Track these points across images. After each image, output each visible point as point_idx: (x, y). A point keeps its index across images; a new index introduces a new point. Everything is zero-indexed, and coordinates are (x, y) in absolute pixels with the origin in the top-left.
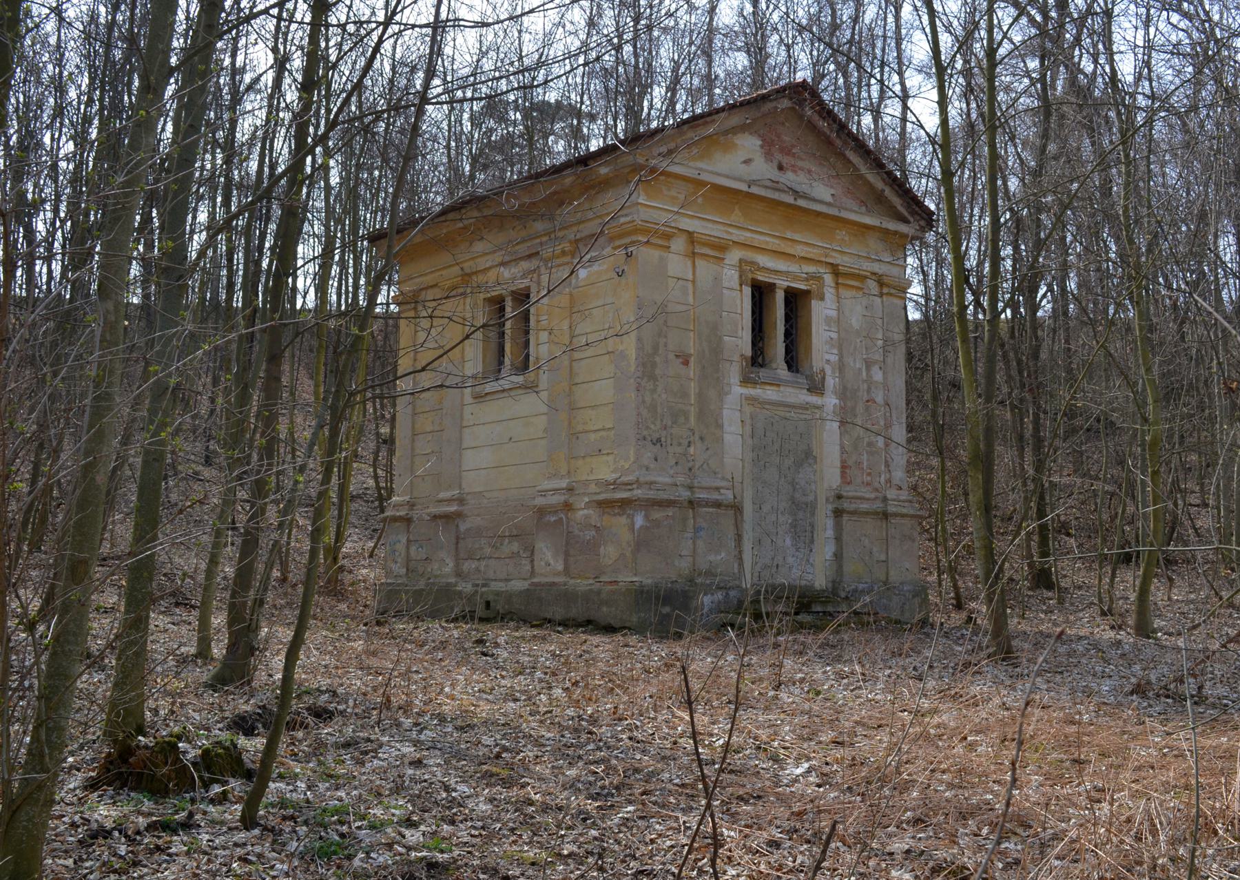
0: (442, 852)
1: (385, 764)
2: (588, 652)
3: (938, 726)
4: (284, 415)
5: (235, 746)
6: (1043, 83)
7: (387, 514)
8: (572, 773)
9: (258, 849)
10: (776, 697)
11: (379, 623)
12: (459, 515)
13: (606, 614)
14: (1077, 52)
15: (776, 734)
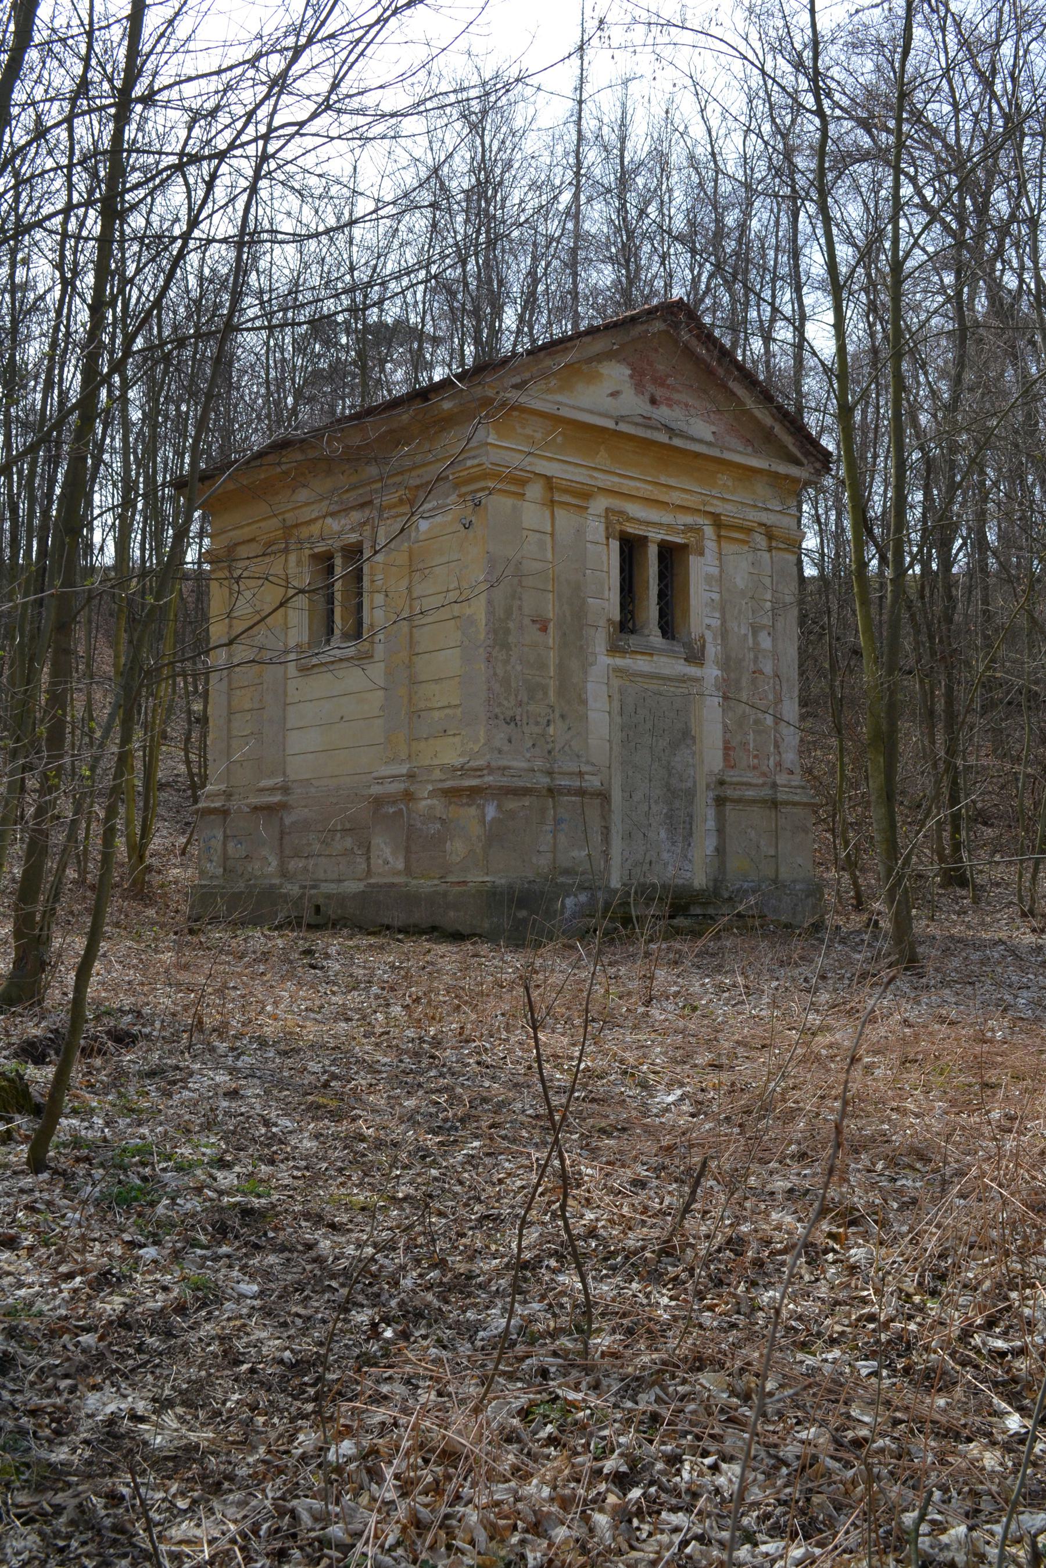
0: (259, 1196)
1: (196, 1095)
2: (432, 964)
3: (830, 1046)
4: (80, 690)
5: (21, 1077)
6: (959, 304)
7: (200, 805)
8: (410, 1103)
9: (46, 1196)
10: (646, 1014)
11: (191, 932)
12: (283, 806)
13: (452, 919)
14: (999, 266)
15: (645, 1056)
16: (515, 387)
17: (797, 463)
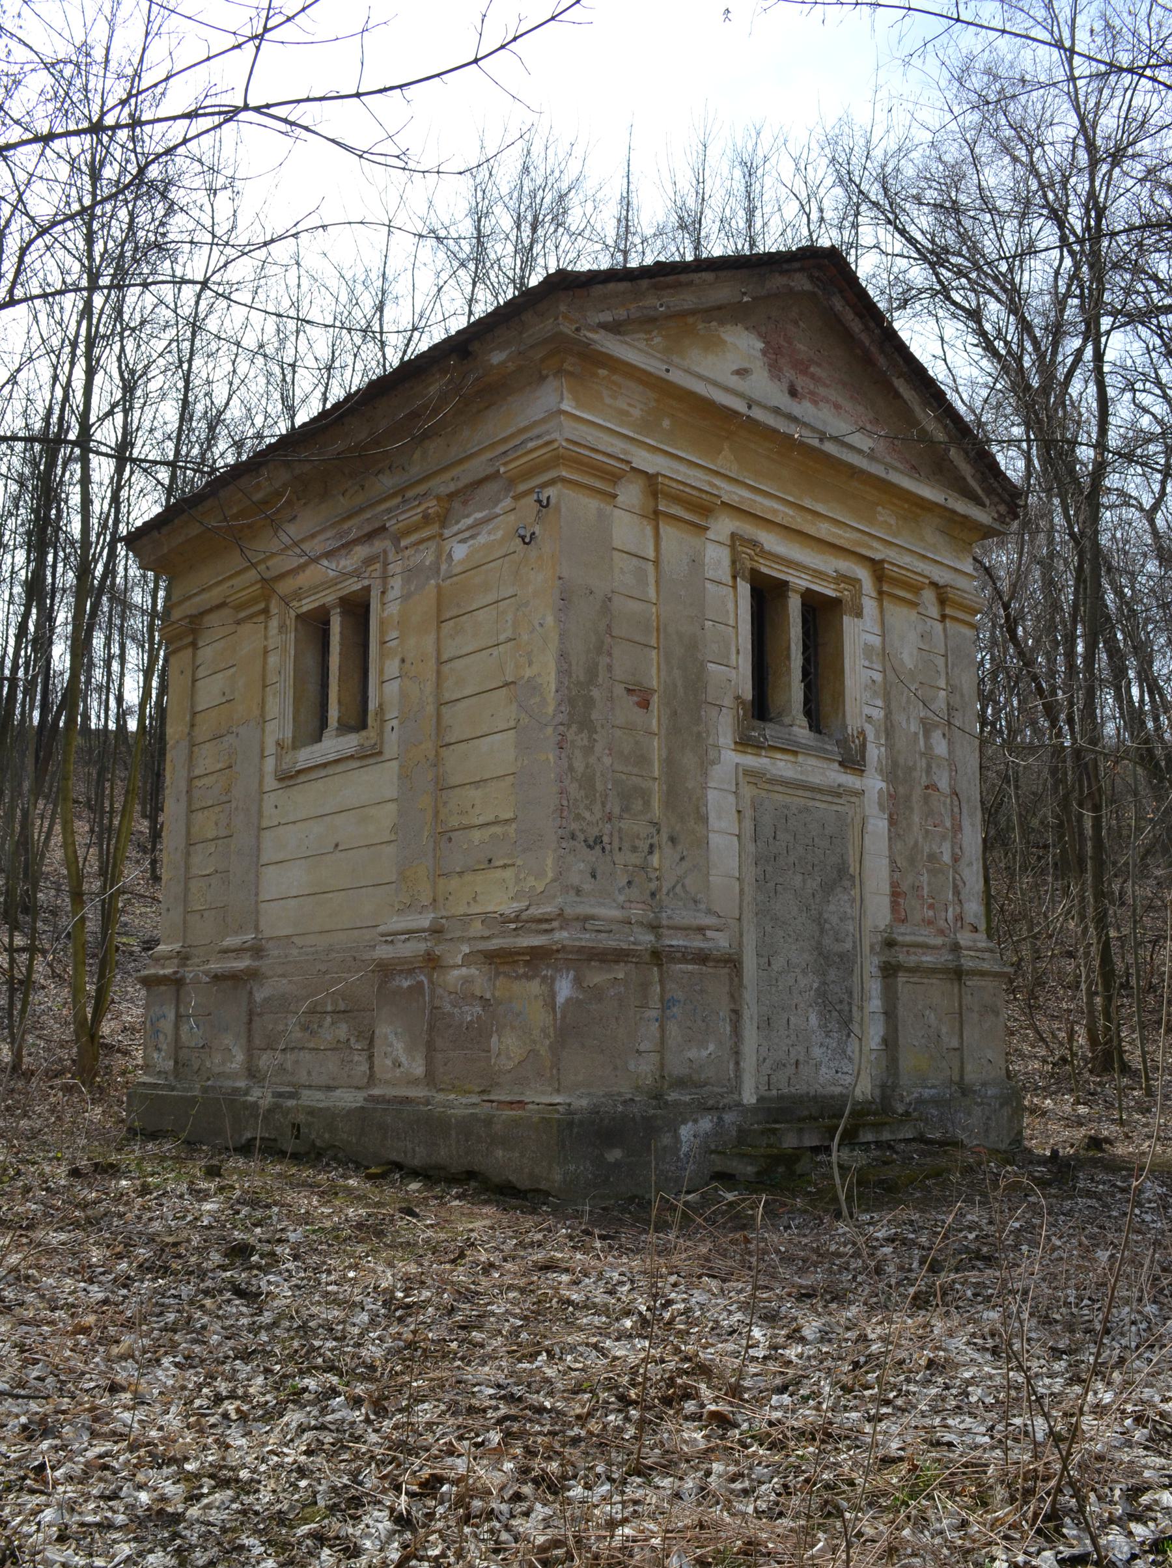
12: (253, 975)
13: (502, 1161)
16: (604, 326)
17: (979, 503)
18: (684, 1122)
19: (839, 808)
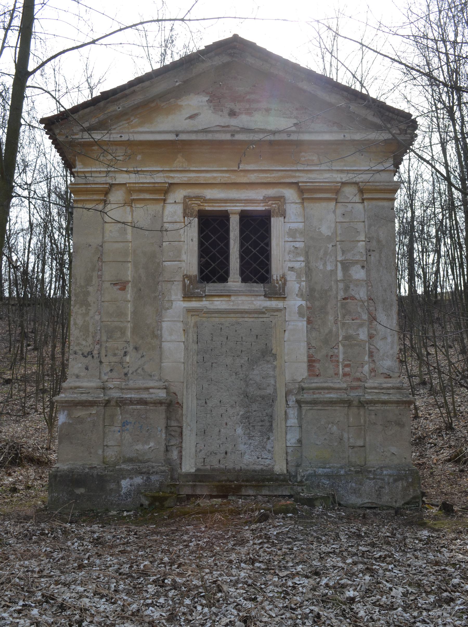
18: (124, 478)
19: (265, 319)
